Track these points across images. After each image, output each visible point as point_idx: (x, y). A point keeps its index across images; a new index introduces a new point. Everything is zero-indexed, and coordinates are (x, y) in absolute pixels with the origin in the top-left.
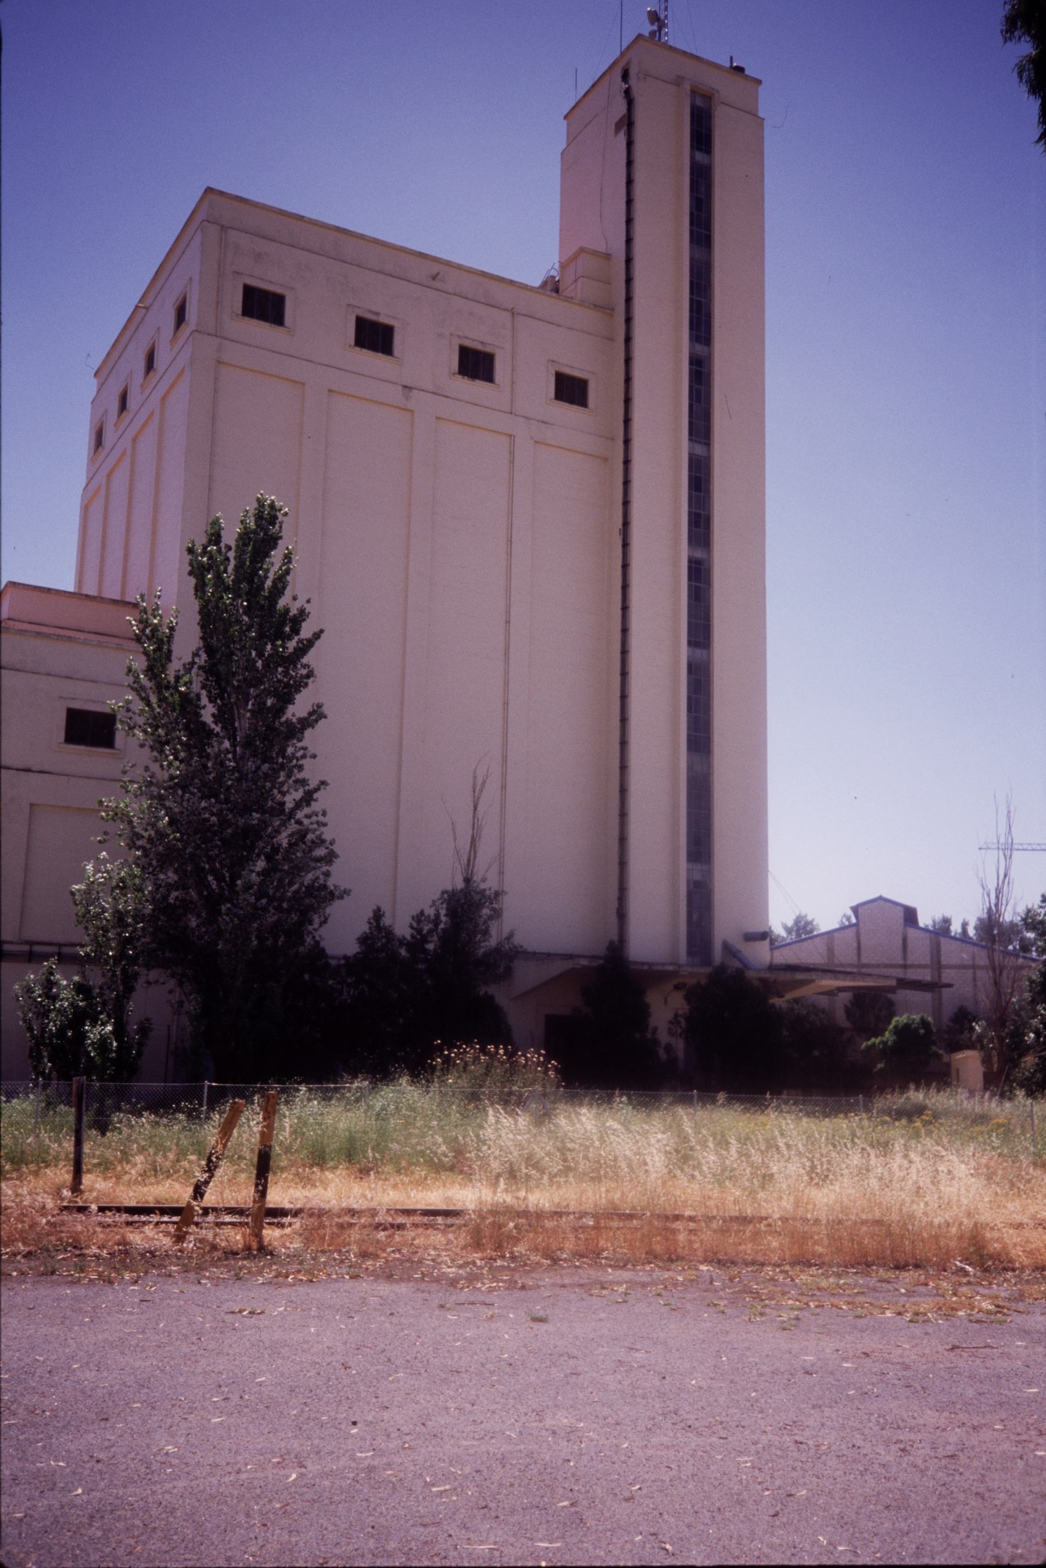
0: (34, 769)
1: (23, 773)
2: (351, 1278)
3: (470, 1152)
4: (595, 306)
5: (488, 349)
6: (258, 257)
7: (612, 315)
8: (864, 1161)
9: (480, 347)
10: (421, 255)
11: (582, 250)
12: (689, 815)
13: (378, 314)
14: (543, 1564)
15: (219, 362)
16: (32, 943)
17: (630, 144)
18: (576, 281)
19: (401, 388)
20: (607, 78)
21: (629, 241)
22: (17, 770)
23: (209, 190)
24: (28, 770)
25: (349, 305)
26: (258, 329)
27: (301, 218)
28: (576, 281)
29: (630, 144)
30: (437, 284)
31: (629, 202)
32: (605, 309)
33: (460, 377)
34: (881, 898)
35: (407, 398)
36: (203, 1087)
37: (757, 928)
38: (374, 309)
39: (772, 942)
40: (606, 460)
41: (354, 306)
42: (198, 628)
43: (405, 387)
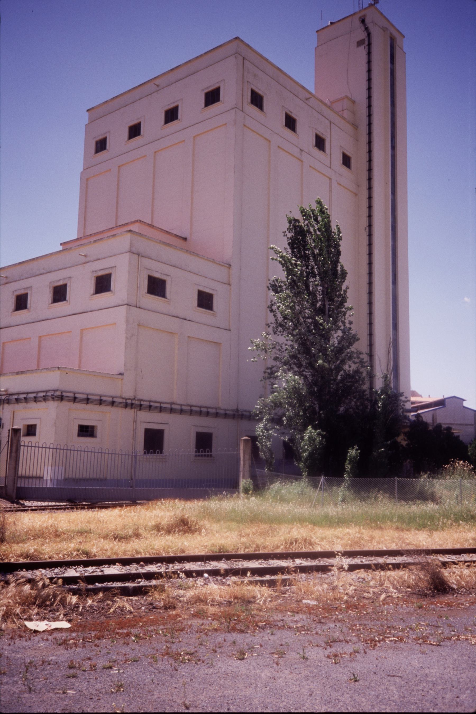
2: (177, 572)
3: (355, 508)
4: (353, 124)
6: (255, 76)
7: (356, 129)
8: (86, 507)
11: (347, 97)
13: (292, 112)
14: (118, 712)
15: (244, 125)
16: (191, 406)
17: (369, 53)
18: (343, 110)
19: (299, 150)
20: (349, 20)
21: (369, 97)
23: (237, 38)
24: (186, 319)
25: (283, 106)
27: (267, 60)
29: (369, 53)
30: (307, 102)
32: (355, 126)
34: (454, 397)
35: (301, 154)
36: (394, 480)
40: (356, 195)
42: (341, 250)
43: (300, 149)
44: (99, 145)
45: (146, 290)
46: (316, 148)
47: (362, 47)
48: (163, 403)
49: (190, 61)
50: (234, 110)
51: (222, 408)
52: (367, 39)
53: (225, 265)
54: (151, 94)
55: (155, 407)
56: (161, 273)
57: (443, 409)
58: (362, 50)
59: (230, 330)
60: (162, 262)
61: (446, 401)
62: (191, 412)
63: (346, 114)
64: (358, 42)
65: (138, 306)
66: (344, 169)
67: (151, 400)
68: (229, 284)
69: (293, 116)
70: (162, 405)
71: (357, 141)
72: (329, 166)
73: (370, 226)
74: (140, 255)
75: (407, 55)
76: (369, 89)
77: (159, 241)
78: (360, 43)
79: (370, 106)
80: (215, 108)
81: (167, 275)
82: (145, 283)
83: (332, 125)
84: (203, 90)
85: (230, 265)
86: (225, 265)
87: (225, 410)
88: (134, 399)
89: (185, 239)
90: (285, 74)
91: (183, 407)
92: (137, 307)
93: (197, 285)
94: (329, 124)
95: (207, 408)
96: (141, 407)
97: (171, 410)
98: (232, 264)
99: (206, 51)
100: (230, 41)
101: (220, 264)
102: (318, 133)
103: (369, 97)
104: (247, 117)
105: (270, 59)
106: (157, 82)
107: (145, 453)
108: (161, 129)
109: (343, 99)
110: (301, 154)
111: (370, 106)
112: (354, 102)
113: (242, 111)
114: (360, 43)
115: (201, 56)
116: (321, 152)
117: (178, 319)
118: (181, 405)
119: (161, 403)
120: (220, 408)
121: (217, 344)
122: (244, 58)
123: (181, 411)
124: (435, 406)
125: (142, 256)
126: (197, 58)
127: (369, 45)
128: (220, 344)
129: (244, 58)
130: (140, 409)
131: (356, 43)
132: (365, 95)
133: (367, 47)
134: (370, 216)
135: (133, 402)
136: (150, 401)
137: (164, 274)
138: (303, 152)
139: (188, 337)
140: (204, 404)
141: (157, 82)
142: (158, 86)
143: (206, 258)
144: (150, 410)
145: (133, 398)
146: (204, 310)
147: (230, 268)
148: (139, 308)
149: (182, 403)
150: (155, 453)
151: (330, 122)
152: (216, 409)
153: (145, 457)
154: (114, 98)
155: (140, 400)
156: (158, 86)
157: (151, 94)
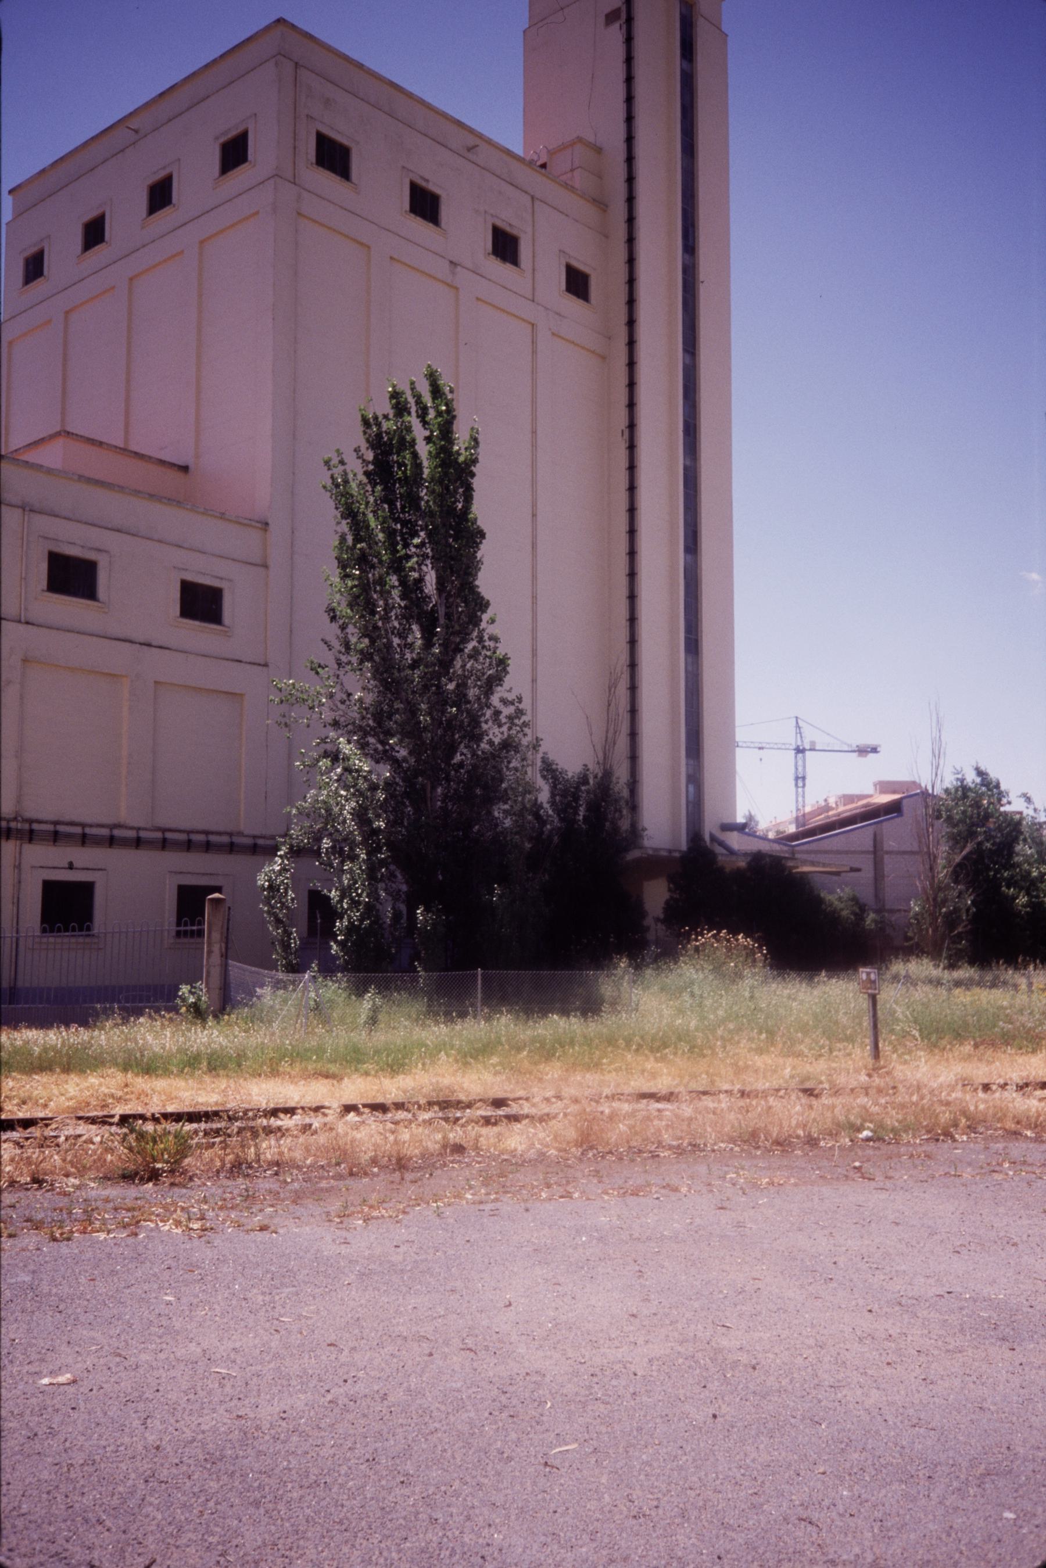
0: (154, 643)
1: (145, 648)
4: (594, 200)
5: (514, 232)
6: (327, 102)
7: (605, 211)
9: (508, 229)
10: (459, 124)
11: (580, 140)
12: (686, 711)
13: (427, 181)
15: (299, 214)
16: (164, 830)
17: (629, 40)
18: (572, 170)
21: (630, 140)
22: (141, 644)
23: (280, 21)
24: (149, 645)
25: (403, 167)
26: (326, 180)
27: (360, 66)
28: (572, 170)
29: (629, 40)
30: (470, 156)
31: (629, 99)
32: (601, 204)
33: (494, 257)
35: (453, 273)
37: (727, 820)
38: (427, 176)
39: (116, 1065)
40: (603, 358)
41: (408, 170)
42: (475, 486)
43: (451, 262)
44: (31, 267)
45: (44, 584)
46: (493, 257)
47: (616, 26)
48: (91, 826)
49: (194, 75)
50: (272, 181)
51: (246, 832)
52: (624, 9)
53: (254, 524)
54: (122, 151)
55: (69, 836)
56: (83, 547)
57: (898, 820)
58: (616, 34)
59: (266, 665)
60: (86, 523)
61: (905, 802)
62: (164, 844)
63: (579, 180)
64: (607, 16)
65: (23, 620)
66: (572, 304)
67: (61, 819)
68: (265, 566)
69: (432, 187)
70: (88, 830)
71: (607, 237)
72: (530, 297)
73: (632, 426)
74: (27, 509)
75: (729, 38)
76: (630, 119)
77: (76, 478)
78: (611, 17)
79: (630, 159)
80: (241, 176)
81: (99, 550)
82: (42, 568)
83: (537, 203)
84: (217, 138)
85: (267, 524)
86: (254, 524)
87: (255, 837)
88: (15, 819)
89: (185, 469)
90: (410, 95)
91: (142, 834)
92: (20, 622)
93: (179, 569)
94: (529, 203)
95: (207, 833)
96: (31, 836)
97: (112, 841)
98: (270, 522)
99: (223, 50)
100: (267, 29)
101: (240, 523)
102: (499, 224)
103: (630, 140)
104: (305, 194)
105: (368, 63)
106: (134, 124)
107: (44, 931)
108: (142, 228)
109: (572, 144)
110: (453, 273)
111: (630, 159)
112: (599, 150)
113: (295, 183)
114: (611, 17)
115: (214, 62)
116: (509, 266)
117: (128, 644)
118: (138, 829)
119: (83, 825)
120: (240, 834)
121: (236, 697)
122: (296, 63)
123: (138, 843)
124: (886, 814)
125: (31, 510)
126: (207, 66)
127: (630, 20)
128: (241, 695)
129: (296, 63)
130: (30, 840)
131: (603, 18)
132: (622, 135)
133: (624, 27)
134: (631, 405)
135: (13, 825)
136: (56, 823)
137: (91, 549)
138: (459, 269)
139: (156, 682)
140: (201, 826)
141: (134, 124)
142: (136, 131)
143: (202, 510)
144: (55, 841)
145: (12, 816)
146: (197, 623)
147: (266, 530)
148: (27, 623)
149: (142, 825)
150: (66, 930)
151: (533, 197)
152: (230, 834)
153: (45, 940)
154: (56, 162)
155: (31, 821)
156: (136, 131)
157: (122, 151)
